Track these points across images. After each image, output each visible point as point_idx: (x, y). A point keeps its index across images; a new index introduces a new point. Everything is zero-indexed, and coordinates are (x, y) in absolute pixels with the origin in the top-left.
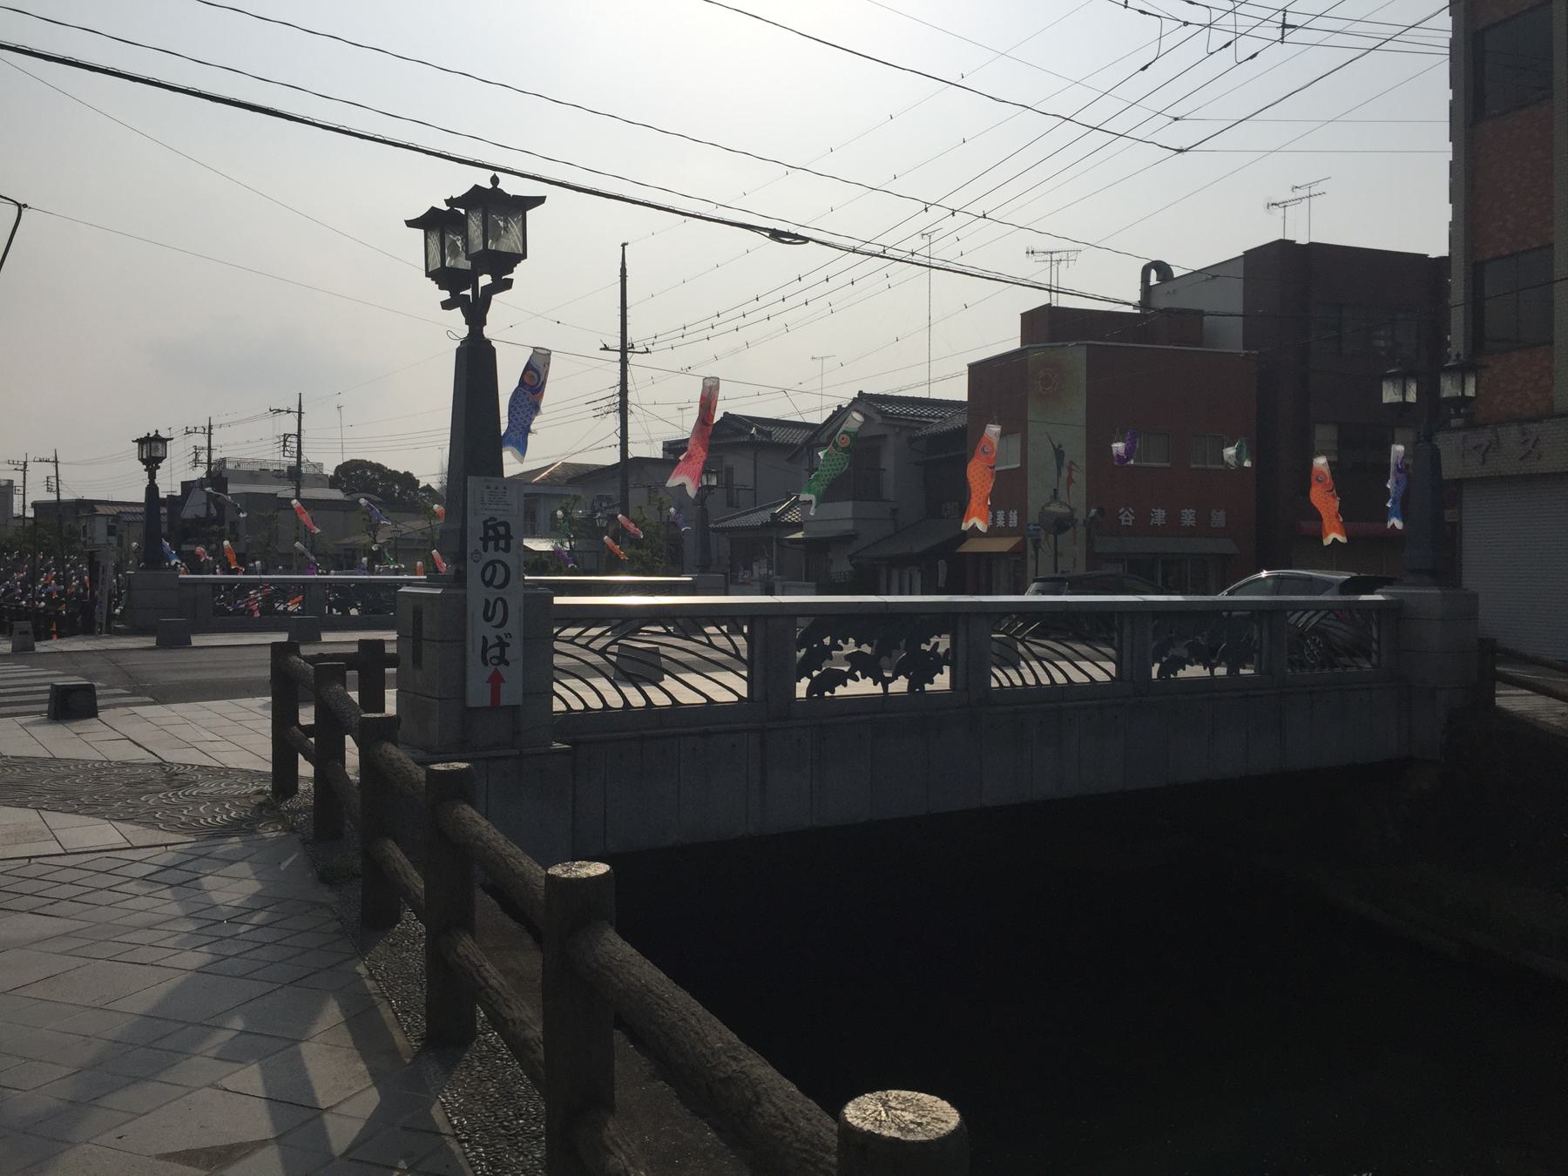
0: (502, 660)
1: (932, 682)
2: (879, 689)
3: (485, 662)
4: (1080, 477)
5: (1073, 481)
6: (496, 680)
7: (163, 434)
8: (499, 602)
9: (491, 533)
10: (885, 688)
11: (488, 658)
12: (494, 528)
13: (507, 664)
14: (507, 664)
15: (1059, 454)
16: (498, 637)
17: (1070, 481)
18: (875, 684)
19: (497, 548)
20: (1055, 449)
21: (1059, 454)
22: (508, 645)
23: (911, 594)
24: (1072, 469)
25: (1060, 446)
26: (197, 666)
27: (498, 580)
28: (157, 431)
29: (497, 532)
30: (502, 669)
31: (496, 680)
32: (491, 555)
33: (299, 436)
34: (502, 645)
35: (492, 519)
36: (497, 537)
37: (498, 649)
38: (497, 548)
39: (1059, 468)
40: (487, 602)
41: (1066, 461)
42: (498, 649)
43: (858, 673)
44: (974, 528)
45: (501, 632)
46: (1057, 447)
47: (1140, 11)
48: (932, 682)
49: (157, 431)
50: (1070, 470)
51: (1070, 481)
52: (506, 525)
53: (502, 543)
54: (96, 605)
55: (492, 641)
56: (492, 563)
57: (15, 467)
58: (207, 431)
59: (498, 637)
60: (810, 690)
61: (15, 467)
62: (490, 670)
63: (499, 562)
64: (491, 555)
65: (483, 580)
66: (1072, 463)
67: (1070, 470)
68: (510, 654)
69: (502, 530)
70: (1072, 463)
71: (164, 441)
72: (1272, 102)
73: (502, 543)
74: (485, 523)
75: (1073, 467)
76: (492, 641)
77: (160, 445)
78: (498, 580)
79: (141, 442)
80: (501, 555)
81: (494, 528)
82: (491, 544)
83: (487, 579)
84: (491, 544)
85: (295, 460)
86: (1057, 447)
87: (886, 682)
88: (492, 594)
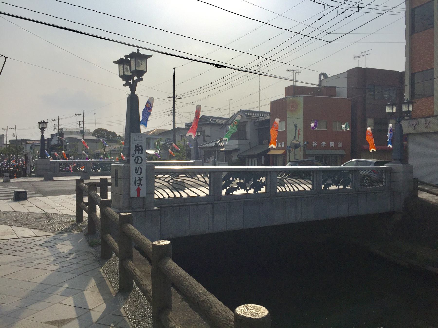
0: (140, 184)
3: (135, 184)
4: (302, 133)
6: (138, 190)
7: (46, 121)
9: (137, 149)
12: (138, 147)
13: (142, 185)
14: (142, 185)
15: (296, 127)
17: (299, 134)
19: (139, 153)
20: (295, 125)
21: (296, 127)
22: (142, 180)
24: (299, 131)
25: (296, 124)
27: (139, 162)
28: (44, 120)
30: (140, 187)
31: (138, 190)
32: (137, 155)
33: (83, 122)
34: (140, 180)
35: (137, 145)
36: (139, 150)
38: (139, 153)
40: (136, 168)
41: (298, 129)
45: (140, 176)
49: (44, 120)
50: (299, 131)
51: (299, 134)
53: (140, 152)
55: (137, 179)
56: (138, 157)
57: (4, 130)
58: (58, 120)
61: (4, 130)
62: (137, 187)
63: (139, 157)
64: (137, 155)
66: (299, 129)
67: (299, 131)
68: (142, 182)
69: (140, 148)
70: (299, 129)
71: (46, 123)
73: (140, 152)
74: (135, 146)
76: (137, 179)
78: (139, 162)
79: (39, 123)
80: (140, 155)
81: (138, 147)
82: (137, 152)
84: (137, 152)
85: (83, 128)
88: (137, 165)
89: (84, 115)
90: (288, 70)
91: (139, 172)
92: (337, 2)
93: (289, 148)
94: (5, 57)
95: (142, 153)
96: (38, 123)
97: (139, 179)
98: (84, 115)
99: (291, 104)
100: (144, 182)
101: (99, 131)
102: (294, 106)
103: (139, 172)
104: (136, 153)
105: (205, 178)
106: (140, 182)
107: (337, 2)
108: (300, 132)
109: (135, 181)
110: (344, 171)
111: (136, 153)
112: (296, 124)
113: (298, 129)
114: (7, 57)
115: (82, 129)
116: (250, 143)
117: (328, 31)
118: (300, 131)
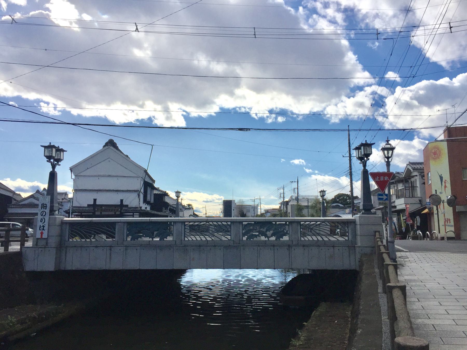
0: (43, 229)
1: (282, 238)
2: (267, 239)
3: (40, 230)
4: (449, 185)
5: (446, 187)
6: (42, 233)
7: (325, 190)
8: (44, 219)
9: (43, 206)
10: (268, 239)
11: (41, 229)
12: (43, 205)
13: (44, 230)
14: (44, 230)
15: (441, 178)
16: (43, 225)
17: (445, 187)
18: (265, 238)
19: (44, 209)
20: (439, 176)
21: (441, 178)
22: (45, 227)
23: (308, 217)
24: (446, 183)
25: (441, 175)
26: (310, 245)
27: (44, 215)
28: (323, 189)
29: (44, 206)
30: (43, 231)
31: (42, 233)
32: (43, 210)
33: (298, 188)
34: (43, 227)
35: (43, 203)
36: (44, 207)
37: (43, 227)
38: (44, 209)
39: (442, 183)
40: (41, 219)
41: (444, 180)
42: (43, 227)
43: (260, 235)
44: (348, 200)
45: (43, 224)
46: (440, 175)
47: (384, 39)
48: (282, 238)
49: (323, 189)
50: (445, 183)
51: (445, 187)
52: (46, 204)
53: (45, 208)
54: (407, 235)
55: (42, 226)
56: (43, 211)
57: (252, 201)
58: (283, 189)
59: (43, 225)
60: (247, 239)
61: (252, 201)
62: (41, 231)
63: (44, 211)
64: (43, 210)
65: (41, 214)
66: (445, 180)
67: (445, 183)
68: (45, 228)
69: (45, 205)
70: (445, 180)
71: (325, 191)
72: (2, 103)
73: (45, 208)
74: (42, 204)
75: (446, 182)
76: (42, 226)
77: (324, 193)
78: (44, 215)
79: (320, 192)
80: (45, 210)
81: (43, 205)
82: (43, 208)
83: (42, 214)
84: (43, 208)
85: (297, 195)
86: (440, 175)
87: (268, 238)
88: (42, 217)
89: (298, 182)
90: (439, 111)
91: (43, 222)
92: (392, 39)
93: (429, 204)
94: (152, 145)
95: (46, 209)
96: (320, 192)
97: (42, 226)
98: (298, 182)
99: (433, 151)
100: (46, 228)
101: (341, 197)
102: (437, 153)
103: (43, 222)
104: (42, 209)
105: (305, 238)
106: (43, 228)
107: (392, 39)
108: (446, 184)
109: (40, 227)
110: (276, 223)
111: (42, 209)
112: (441, 175)
113: (444, 181)
114: (153, 145)
115: (297, 196)
116: (420, 201)
117: (412, 68)
118: (447, 182)
